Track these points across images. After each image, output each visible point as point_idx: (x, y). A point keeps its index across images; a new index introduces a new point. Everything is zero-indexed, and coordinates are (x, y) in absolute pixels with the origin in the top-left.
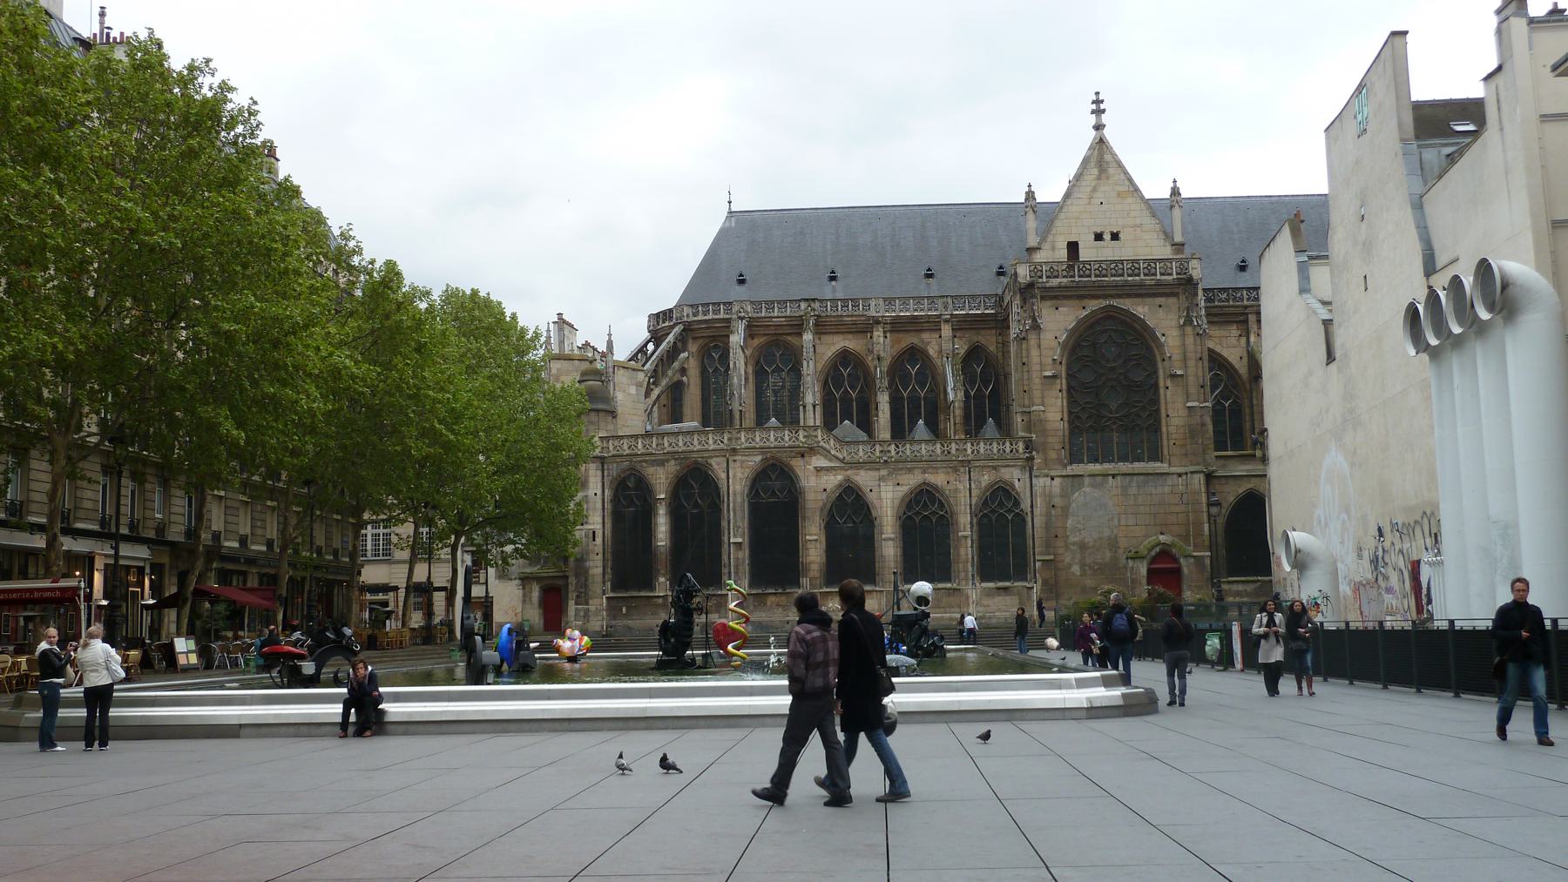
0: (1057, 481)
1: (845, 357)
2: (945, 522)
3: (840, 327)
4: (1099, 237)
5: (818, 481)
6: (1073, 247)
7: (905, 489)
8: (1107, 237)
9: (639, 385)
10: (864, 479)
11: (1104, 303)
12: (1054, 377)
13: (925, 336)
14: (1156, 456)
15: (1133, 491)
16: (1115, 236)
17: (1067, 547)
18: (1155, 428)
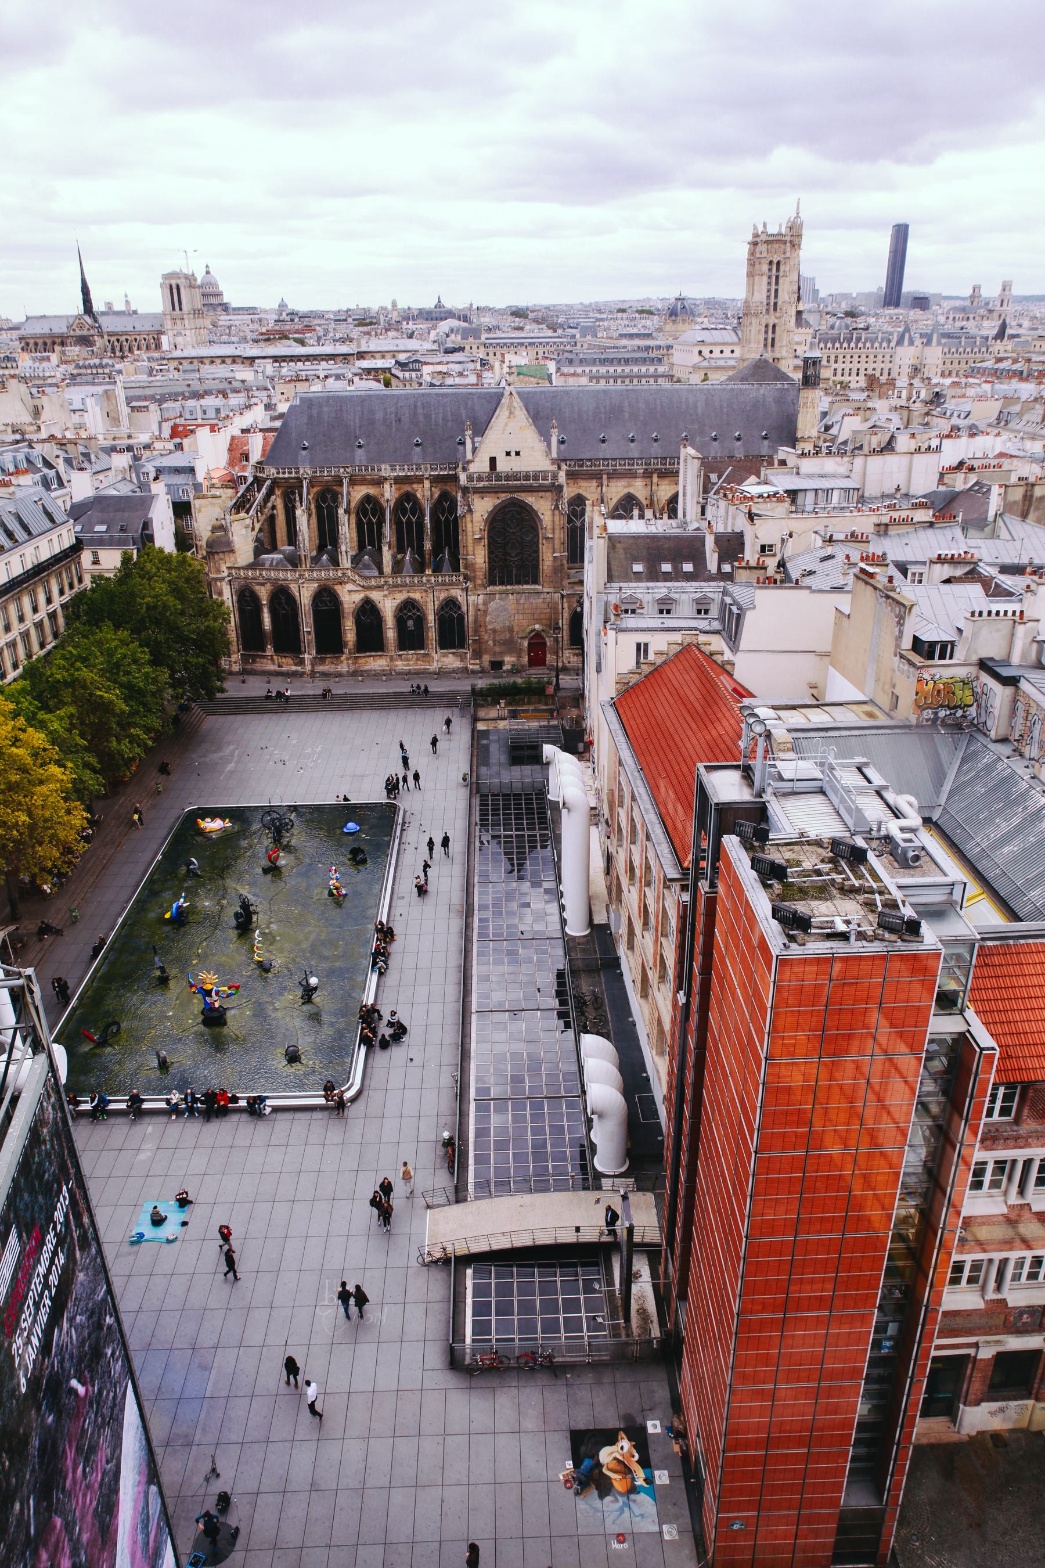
0: (481, 596)
1: (368, 498)
2: (420, 621)
3: (364, 482)
4: (508, 454)
5: (350, 597)
6: (493, 461)
7: (398, 601)
8: (513, 454)
9: (247, 527)
10: (375, 596)
11: (510, 496)
12: (480, 539)
13: (415, 486)
14: (536, 582)
15: (522, 601)
16: (518, 454)
17: (486, 631)
18: (536, 567)
